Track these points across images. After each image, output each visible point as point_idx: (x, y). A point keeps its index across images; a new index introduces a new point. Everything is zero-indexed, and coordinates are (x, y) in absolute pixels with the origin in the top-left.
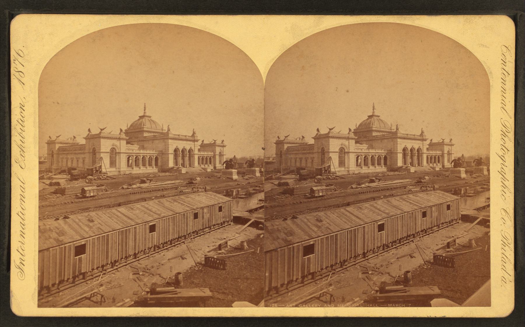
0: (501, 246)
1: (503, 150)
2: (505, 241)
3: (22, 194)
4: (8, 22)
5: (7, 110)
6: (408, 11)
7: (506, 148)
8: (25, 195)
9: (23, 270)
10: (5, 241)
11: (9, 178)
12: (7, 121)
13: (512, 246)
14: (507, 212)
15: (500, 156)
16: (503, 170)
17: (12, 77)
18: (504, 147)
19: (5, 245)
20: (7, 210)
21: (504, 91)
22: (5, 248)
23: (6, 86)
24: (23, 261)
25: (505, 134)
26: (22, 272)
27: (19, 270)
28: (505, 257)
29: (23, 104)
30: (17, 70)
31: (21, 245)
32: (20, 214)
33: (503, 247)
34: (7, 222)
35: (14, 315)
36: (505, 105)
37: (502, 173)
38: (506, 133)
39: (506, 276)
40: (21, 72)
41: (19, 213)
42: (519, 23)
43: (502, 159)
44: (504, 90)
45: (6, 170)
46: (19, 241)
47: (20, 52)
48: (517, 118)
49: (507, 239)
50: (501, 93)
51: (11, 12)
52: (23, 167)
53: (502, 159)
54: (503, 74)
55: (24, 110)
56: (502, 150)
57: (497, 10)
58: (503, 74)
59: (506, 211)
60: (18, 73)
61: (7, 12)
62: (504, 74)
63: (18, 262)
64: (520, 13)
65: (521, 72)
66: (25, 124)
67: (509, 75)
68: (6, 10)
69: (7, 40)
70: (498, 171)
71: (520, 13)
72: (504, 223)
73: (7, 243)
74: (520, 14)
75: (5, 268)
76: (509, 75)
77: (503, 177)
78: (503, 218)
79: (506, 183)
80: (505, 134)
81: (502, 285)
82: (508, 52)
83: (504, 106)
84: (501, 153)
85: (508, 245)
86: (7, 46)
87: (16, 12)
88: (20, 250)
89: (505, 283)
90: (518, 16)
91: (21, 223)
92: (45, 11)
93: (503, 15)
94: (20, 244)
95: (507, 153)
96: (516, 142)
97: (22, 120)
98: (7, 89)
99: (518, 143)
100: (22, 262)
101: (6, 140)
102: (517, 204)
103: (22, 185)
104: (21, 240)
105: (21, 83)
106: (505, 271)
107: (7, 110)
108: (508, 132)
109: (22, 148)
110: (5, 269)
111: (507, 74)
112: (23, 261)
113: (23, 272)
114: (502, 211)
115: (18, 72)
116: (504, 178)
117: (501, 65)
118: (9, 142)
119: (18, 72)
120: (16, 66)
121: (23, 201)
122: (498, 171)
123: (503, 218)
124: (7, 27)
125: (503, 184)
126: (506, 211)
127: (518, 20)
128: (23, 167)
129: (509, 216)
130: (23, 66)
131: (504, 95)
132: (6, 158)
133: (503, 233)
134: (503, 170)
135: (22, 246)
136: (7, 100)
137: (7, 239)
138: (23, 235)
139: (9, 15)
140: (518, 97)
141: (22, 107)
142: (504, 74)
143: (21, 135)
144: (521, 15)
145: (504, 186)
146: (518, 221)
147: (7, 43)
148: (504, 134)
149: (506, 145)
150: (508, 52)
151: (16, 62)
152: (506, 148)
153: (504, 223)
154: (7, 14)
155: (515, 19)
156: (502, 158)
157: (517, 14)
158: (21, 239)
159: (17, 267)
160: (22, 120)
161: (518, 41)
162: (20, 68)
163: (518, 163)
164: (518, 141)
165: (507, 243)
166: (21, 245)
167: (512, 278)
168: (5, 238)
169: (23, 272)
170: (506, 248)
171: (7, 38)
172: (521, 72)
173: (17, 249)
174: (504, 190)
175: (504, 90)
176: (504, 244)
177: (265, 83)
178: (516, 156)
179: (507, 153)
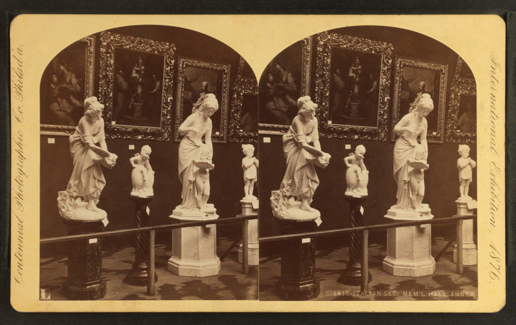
0: (23, 85)
4: (8, 23)
5: (8, 109)
7: (18, 182)
8: (490, 137)
9: (491, 61)
10: (6, 238)
13: (12, 85)
16: (21, 160)
21: (20, 239)
24: (492, 71)
25: (19, 196)
26: (494, 61)
27: (495, 62)
28: (19, 74)
29: (491, 225)
33: (20, 84)
36: (19, 224)
40: (494, 258)
43: (22, 172)
44: (19, 239)
53: (22, 172)
54: (21, 256)
57: (488, 9)
58: (21, 254)
59: (18, 120)
60: (496, 257)
61: (7, 13)
62: (20, 254)
63: (497, 71)
66: (490, 206)
72: (20, 108)
73: (8, 239)
74: (510, 13)
75: (6, 263)
77: (492, 182)
78: (21, 113)
79: (18, 148)
80: (19, 196)
81: (21, 46)
83: (20, 223)
84: (23, 177)
90: (508, 15)
93: (496, 14)
94: (495, 88)
95: (17, 177)
96: (507, 138)
97: (493, 209)
98: (7, 88)
103: (493, 146)
105: (493, 247)
106: (19, 60)
107: (8, 109)
108: (16, 198)
112: (492, 71)
114: (21, 120)
115: (495, 258)
119: (495, 258)
125: (21, 148)
126: (18, 120)
127: (508, 19)
128: (492, 164)
129: (15, 115)
131: (20, 235)
133: (21, 99)
135: (493, 86)
142: (20, 254)
143: (494, 196)
144: (511, 14)
145: (19, 144)
148: (20, 195)
149: (18, 185)
152: (18, 182)
153: (20, 108)
154: (8, 15)
155: (505, 18)
156: (22, 172)
157: (506, 14)
158: (494, 93)
159: (498, 65)
160: (493, 209)
161: (508, 39)
162: (494, 261)
165: (17, 88)
167: (12, 53)
170: (18, 83)
173: (498, 83)
174: (20, 141)
175: (19, 239)
179: (17, 177)
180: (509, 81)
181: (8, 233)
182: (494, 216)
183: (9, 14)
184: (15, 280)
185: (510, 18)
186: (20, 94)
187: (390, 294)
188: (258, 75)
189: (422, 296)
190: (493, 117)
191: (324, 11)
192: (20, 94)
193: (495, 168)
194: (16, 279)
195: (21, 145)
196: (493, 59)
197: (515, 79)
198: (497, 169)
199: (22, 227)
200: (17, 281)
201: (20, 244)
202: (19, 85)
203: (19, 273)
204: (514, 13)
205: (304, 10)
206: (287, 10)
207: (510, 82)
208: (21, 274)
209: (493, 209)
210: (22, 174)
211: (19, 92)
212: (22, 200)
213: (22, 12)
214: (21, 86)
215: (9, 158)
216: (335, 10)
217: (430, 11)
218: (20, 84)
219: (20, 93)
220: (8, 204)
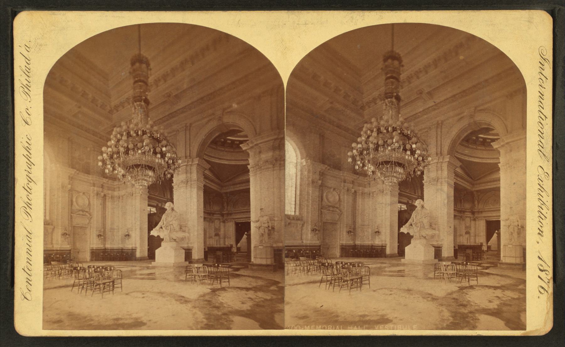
1: (28, 188)
2: (26, 90)
4: (10, 20)
6: (438, 6)
7: (26, 190)
8: (538, 138)
10: (9, 255)
11: (13, 187)
12: (10, 126)
14: (25, 121)
15: (33, 182)
17: (550, 264)
18: (28, 190)
19: (9, 258)
20: (10, 222)
21: (29, 252)
22: (9, 261)
23: (10, 88)
25: (28, 206)
30: (546, 272)
31: (542, 84)
33: (28, 84)
34: (11, 234)
35: (18, 335)
36: (27, 236)
37: (30, 164)
38: (26, 206)
39: (25, 53)
41: (544, 119)
42: (557, 18)
45: (9, 178)
46: (545, 88)
47: (542, 290)
48: (555, 119)
49: (24, 92)
50: (32, 249)
51: (14, 9)
52: (540, 169)
55: (539, 229)
56: (31, 188)
57: (534, 4)
58: (30, 269)
61: (9, 9)
62: (28, 269)
64: (558, 7)
65: (560, 64)
67: (23, 269)
68: (8, 7)
69: (10, 39)
70: (34, 165)
71: (558, 7)
73: (10, 256)
75: (9, 283)
76: (23, 269)
77: (540, 188)
78: (29, 115)
79: (26, 153)
80: (28, 206)
82: (25, 293)
84: (32, 185)
85: (23, 86)
86: (10, 46)
87: (19, 9)
88: (544, 79)
92: (50, 8)
96: (555, 145)
98: (10, 92)
99: (557, 146)
100: (541, 66)
101: (9, 147)
102: (556, 212)
104: (543, 89)
107: (10, 114)
110: (9, 284)
111: (25, 270)
113: (541, 56)
114: (30, 123)
116: (28, 158)
117: (32, 278)
118: (13, 148)
120: (547, 276)
122: (34, 165)
123: (29, 115)
124: (10, 25)
126: (26, 123)
132: (9, 166)
133: (30, 220)
134: (30, 167)
136: (11, 103)
137: (10, 253)
138: (541, 96)
139: (11, 13)
140: (557, 98)
141: (541, 233)
142: (28, 269)
143: (542, 203)
144: (559, 10)
145: (28, 149)
146: (557, 230)
147: (9, 42)
149: (26, 193)
150: (25, 293)
151: (547, 281)
152: (26, 190)
154: (10, 11)
155: (552, 13)
156: (30, 180)
157: (555, 8)
159: (546, 60)
162: (543, 275)
163: (557, 168)
164: (557, 144)
166: (542, 84)
168: (9, 251)
169: (541, 56)
170: (25, 82)
171: (10, 37)
172: (560, 64)
176: (28, 87)
177: (287, 89)
178: (554, 160)
180: (557, 82)
181: (11, 250)
182: (542, 225)
183: (12, 11)
184: (24, 297)
185: (558, 14)
186: (28, 94)
188: (285, 76)
190: (541, 118)
191: (356, 6)
192: (28, 94)
193: (543, 172)
194: (24, 296)
195: (28, 149)
197: (564, 80)
198: (546, 174)
199: (29, 69)
200: (25, 297)
201: (28, 257)
202: (27, 84)
203: (28, 289)
204: (563, 8)
205: (333, 5)
206: (315, 6)
207: (558, 83)
208: (30, 290)
209: (541, 216)
210: (31, 181)
211: (28, 92)
212: (30, 209)
213: (25, 8)
214: (29, 85)
215: (13, 168)
216: (367, 5)
217: (471, 5)
218: (28, 84)
220: (11, 218)
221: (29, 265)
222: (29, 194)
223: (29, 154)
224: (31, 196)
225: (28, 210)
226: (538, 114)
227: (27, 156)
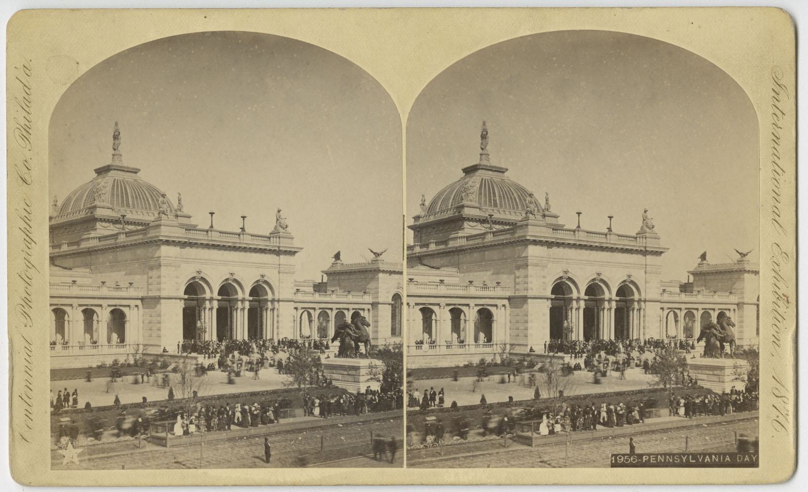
3: (776, 146)
14: (22, 179)
21: (28, 370)
26: (777, 80)
28: (25, 107)
32: (780, 318)
78: (28, 169)
84: (32, 272)
89: (24, 66)
91: (779, 216)
95: (23, 272)
109: (776, 276)
114: (29, 182)
121: (776, 193)
123: (28, 169)
130: (774, 406)
133: (29, 146)
134: (29, 245)
135: (776, 119)
159: (783, 87)
174: (27, 123)
179: (23, 272)
187: (653, 460)
189: (691, 461)
195: (28, 221)
196: (775, 78)
219: (27, 137)
221: (28, 389)
222: (28, 286)
223: (28, 228)
224: (31, 290)
225: (27, 309)
226: (771, 110)
227: (25, 230)
